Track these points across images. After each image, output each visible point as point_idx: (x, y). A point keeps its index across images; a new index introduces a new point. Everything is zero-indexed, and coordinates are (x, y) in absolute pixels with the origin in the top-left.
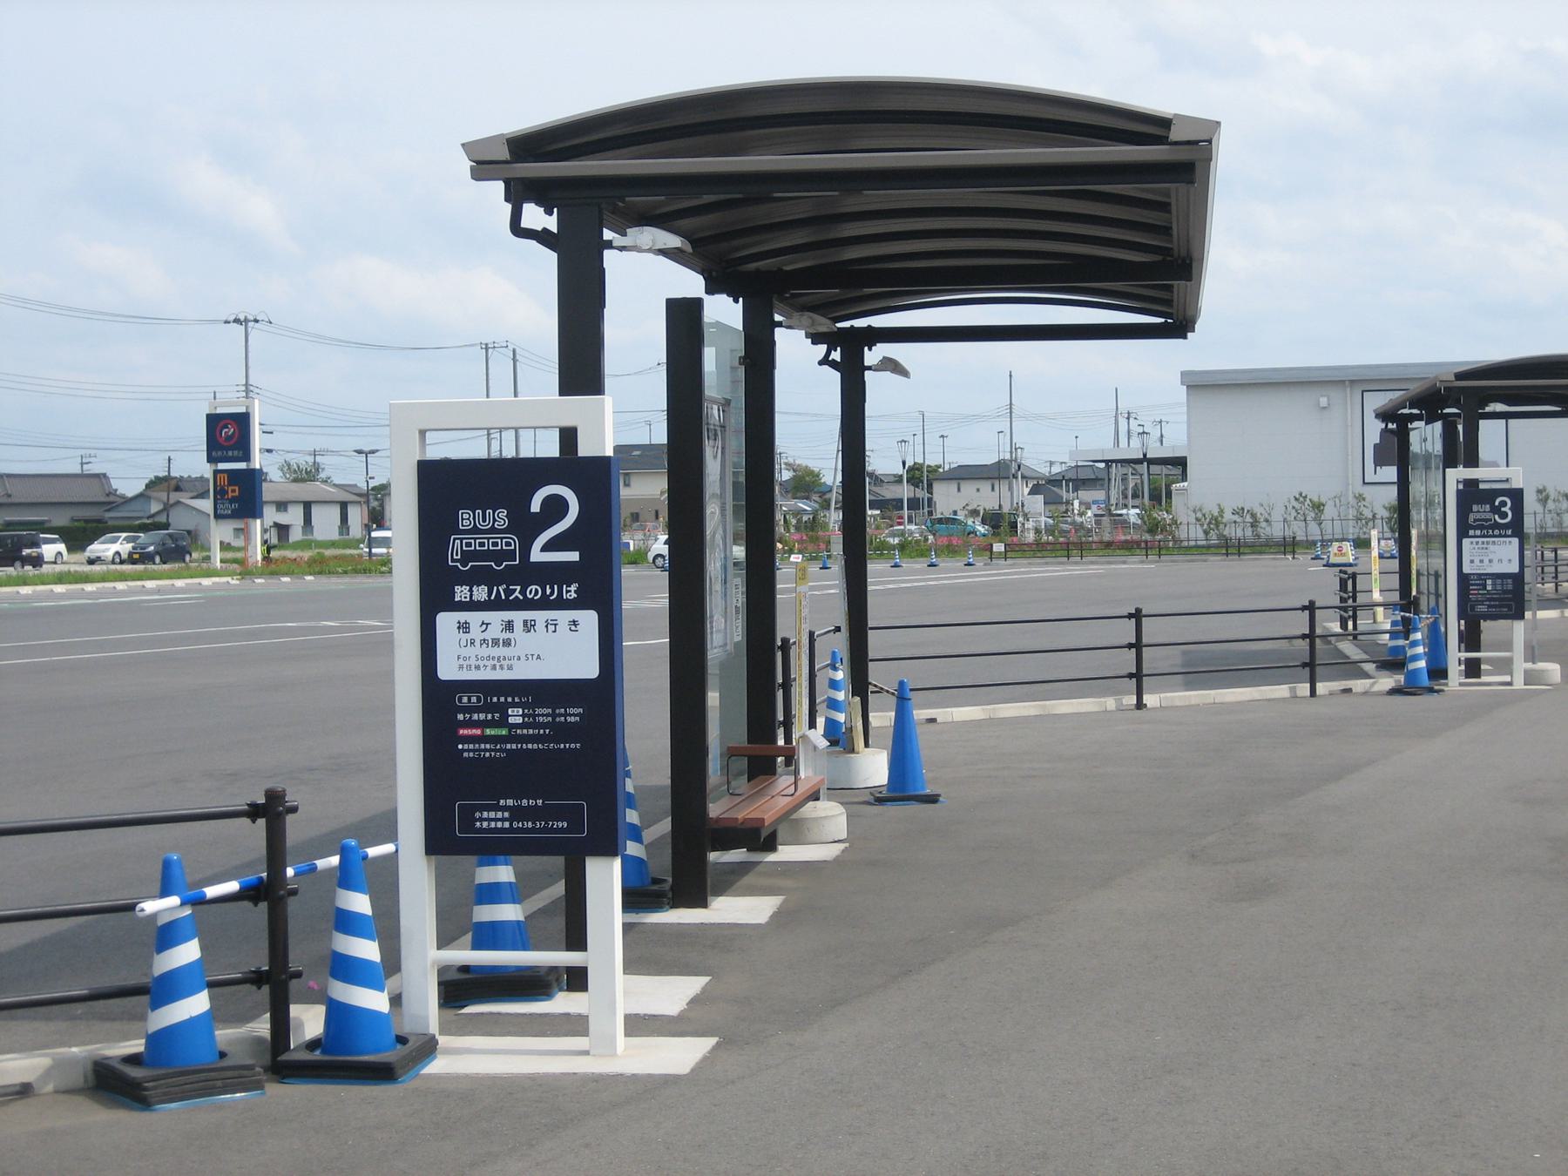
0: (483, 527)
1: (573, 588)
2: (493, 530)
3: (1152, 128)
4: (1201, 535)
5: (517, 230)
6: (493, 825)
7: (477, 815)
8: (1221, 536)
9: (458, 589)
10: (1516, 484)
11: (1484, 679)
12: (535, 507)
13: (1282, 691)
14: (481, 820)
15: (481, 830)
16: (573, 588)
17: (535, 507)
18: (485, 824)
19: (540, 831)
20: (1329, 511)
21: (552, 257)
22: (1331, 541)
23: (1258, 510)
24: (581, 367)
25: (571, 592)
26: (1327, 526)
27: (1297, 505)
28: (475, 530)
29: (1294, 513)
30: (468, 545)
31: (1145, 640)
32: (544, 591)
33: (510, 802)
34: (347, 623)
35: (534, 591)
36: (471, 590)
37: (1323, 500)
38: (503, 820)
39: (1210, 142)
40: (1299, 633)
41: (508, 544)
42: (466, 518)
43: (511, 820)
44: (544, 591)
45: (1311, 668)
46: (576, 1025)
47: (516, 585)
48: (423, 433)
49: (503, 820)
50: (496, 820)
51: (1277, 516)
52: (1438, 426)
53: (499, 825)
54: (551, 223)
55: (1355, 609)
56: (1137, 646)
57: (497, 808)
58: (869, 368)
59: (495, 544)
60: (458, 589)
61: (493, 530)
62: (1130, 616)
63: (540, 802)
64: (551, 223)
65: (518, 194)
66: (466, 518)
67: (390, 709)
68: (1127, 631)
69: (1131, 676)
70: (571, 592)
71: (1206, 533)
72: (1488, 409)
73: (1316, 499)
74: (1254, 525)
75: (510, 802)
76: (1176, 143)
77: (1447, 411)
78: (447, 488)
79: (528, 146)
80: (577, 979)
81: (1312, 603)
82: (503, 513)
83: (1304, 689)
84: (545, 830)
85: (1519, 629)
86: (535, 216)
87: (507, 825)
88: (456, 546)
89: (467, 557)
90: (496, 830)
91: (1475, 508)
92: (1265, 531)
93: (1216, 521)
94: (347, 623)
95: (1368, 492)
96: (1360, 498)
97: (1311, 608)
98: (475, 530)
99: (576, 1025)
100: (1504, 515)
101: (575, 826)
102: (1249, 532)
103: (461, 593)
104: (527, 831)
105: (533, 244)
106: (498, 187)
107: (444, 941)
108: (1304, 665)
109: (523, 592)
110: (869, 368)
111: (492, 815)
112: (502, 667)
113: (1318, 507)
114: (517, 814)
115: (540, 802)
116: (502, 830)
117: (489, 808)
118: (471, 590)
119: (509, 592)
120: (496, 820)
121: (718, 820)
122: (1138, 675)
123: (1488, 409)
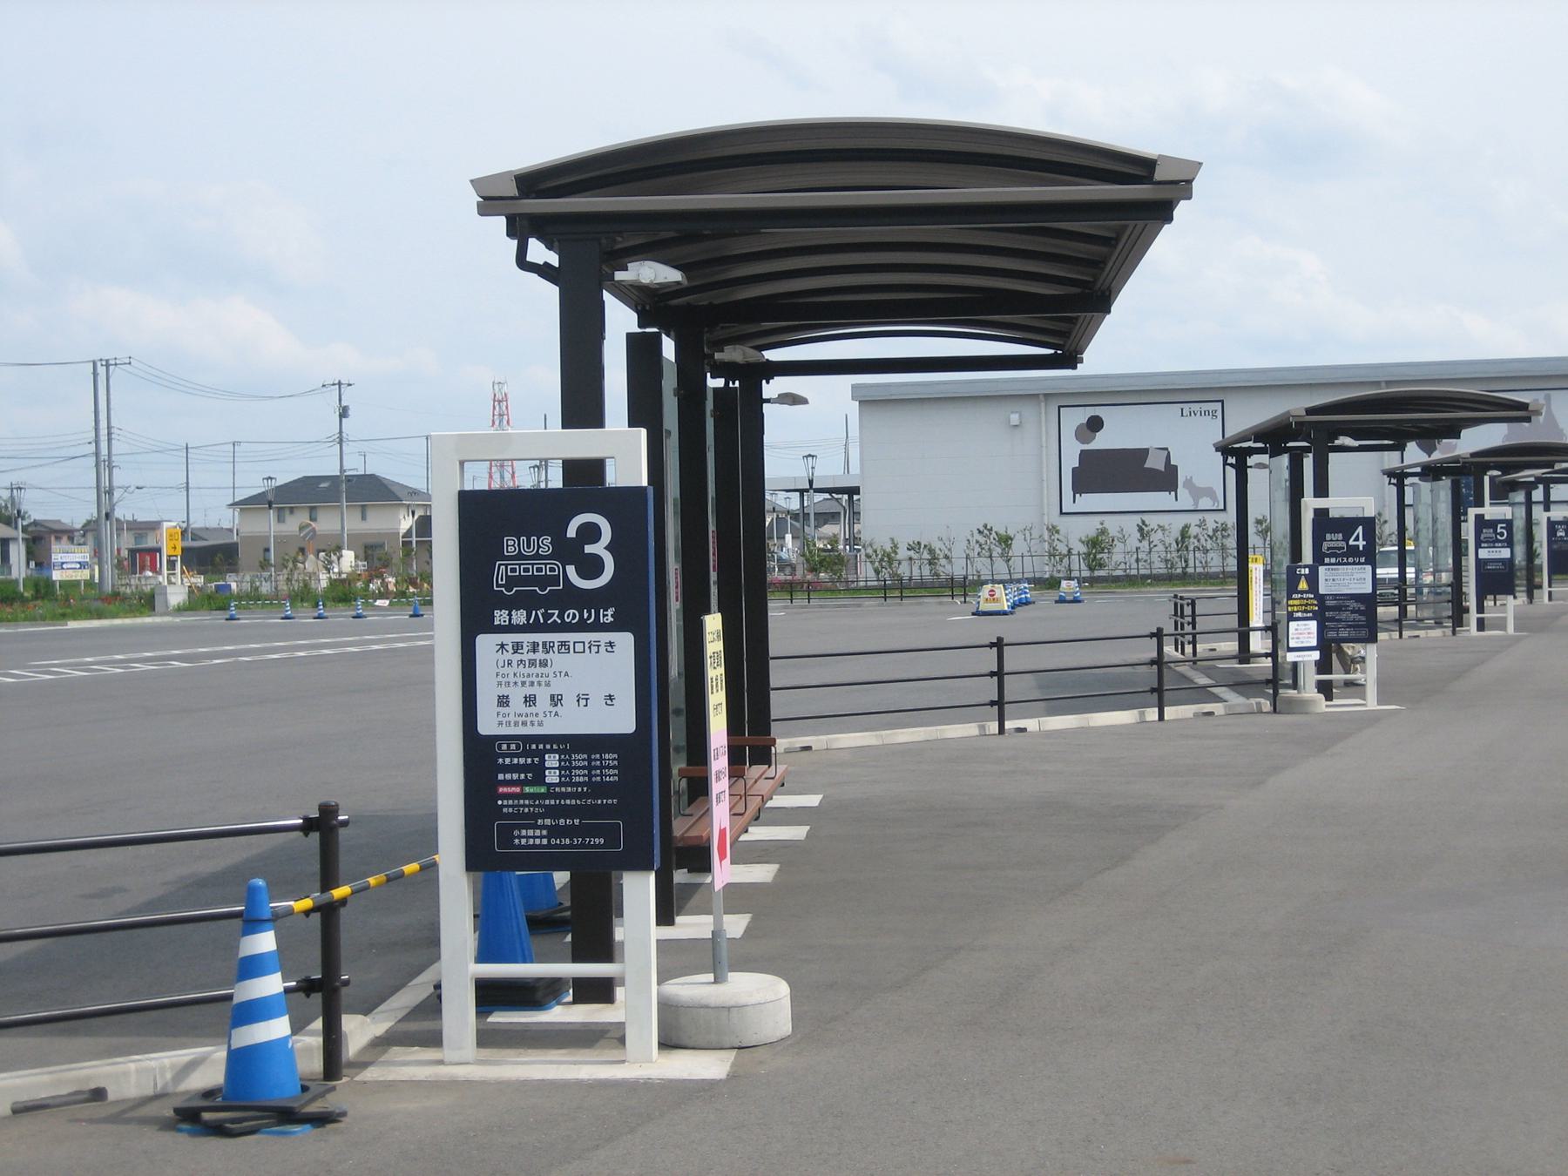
0: (524, 554)
1: (610, 612)
2: (537, 556)
3: (1139, 168)
4: (871, 574)
5: (522, 263)
6: (531, 842)
7: (516, 833)
8: (894, 575)
9: (497, 613)
10: (1370, 512)
11: (1335, 702)
12: (571, 532)
13: (971, 730)
14: (520, 837)
15: (520, 846)
16: (610, 612)
17: (571, 532)
18: (523, 841)
19: (577, 847)
20: (1018, 546)
21: (554, 291)
22: (986, 582)
23: (937, 545)
24: (582, 404)
25: (608, 616)
26: (1016, 563)
27: (982, 540)
28: (520, 556)
29: (977, 549)
30: (513, 570)
31: (1007, 669)
32: (581, 615)
33: (548, 822)
34: (315, 652)
35: (571, 615)
36: (510, 615)
37: (1010, 533)
38: (541, 837)
39: (1189, 182)
40: (986, 670)
41: (552, 570)
42: (511, 545)
43: (549, 837)
44: (581, 615)
45: (1159, 696)
46: (612, 1037)
47: (1493, 543)
48: (462, 463)
49: (541, 837)
50: (534, 837)
51: (958, 552)
52: (1285, 459)
53: (538, 841)
54: (553, 259)
55: (1194, 636)
56: (999, 674)
57: (535, 827)
58: (768, 401)
59: (539, 570)
60: (497, 613)
61: (537, 556)
62: (992, 645)
63: (577, 822)
64: (553, 259)
65: (520, 228)
66: (511, 545)
67: (431, 728)
68: (989, 660)
69: (992, 703)
70: (608, 616)
71: (877, 572)
72: (1337, 442)
73: (1002, 532)
74: (932, 562)
75: (548, 822)
76: (1160, 183)
77: (1291, 444)
78: (489, 517)
79: (533, 182)
80: (600, 991)
81: (1000, 639)
82: (547, 540)
83: (993, 727)
84: (582, 846)
85: (1370, 652)
86: (538, 252)
87: (545, 841)
88: (501, 572)
89: (511, 582)
90: (534, 846)
91: (1328, 536)
92: (945, 569)
93: (889, 558)
94: (315, 652)
95: (1064, 524)
96: (1053, 530)
97: (1158, 635)
98: (520, 556)
99: (612, 1037)
100: (592, 567)
101: (612, 840)
102: (926, 571)
103: (501, 617)
104: (565, 846)
105: (533, 277)
106: (500, 222)
107: (483, 956)
108: (1153, 690)
109: (561, 616)
110: (768, 401)
111: (530, 833)
112: (539, 684)
113: (1006, 541)
114: (554, 832)
115: (577, 822)
116: (541, 846)
117: (527, 827)
118: (510, 615)
119: (547, 616)
120: (534, 837)
121: (683, 838)
122: (999, 703)
123: (1337, 442)
